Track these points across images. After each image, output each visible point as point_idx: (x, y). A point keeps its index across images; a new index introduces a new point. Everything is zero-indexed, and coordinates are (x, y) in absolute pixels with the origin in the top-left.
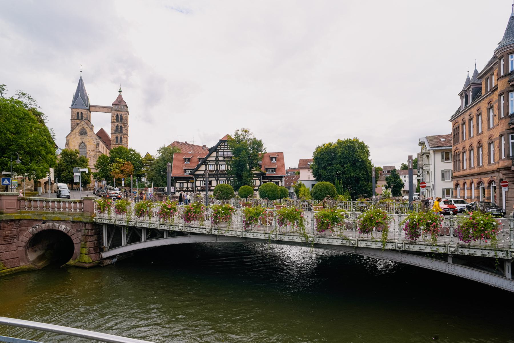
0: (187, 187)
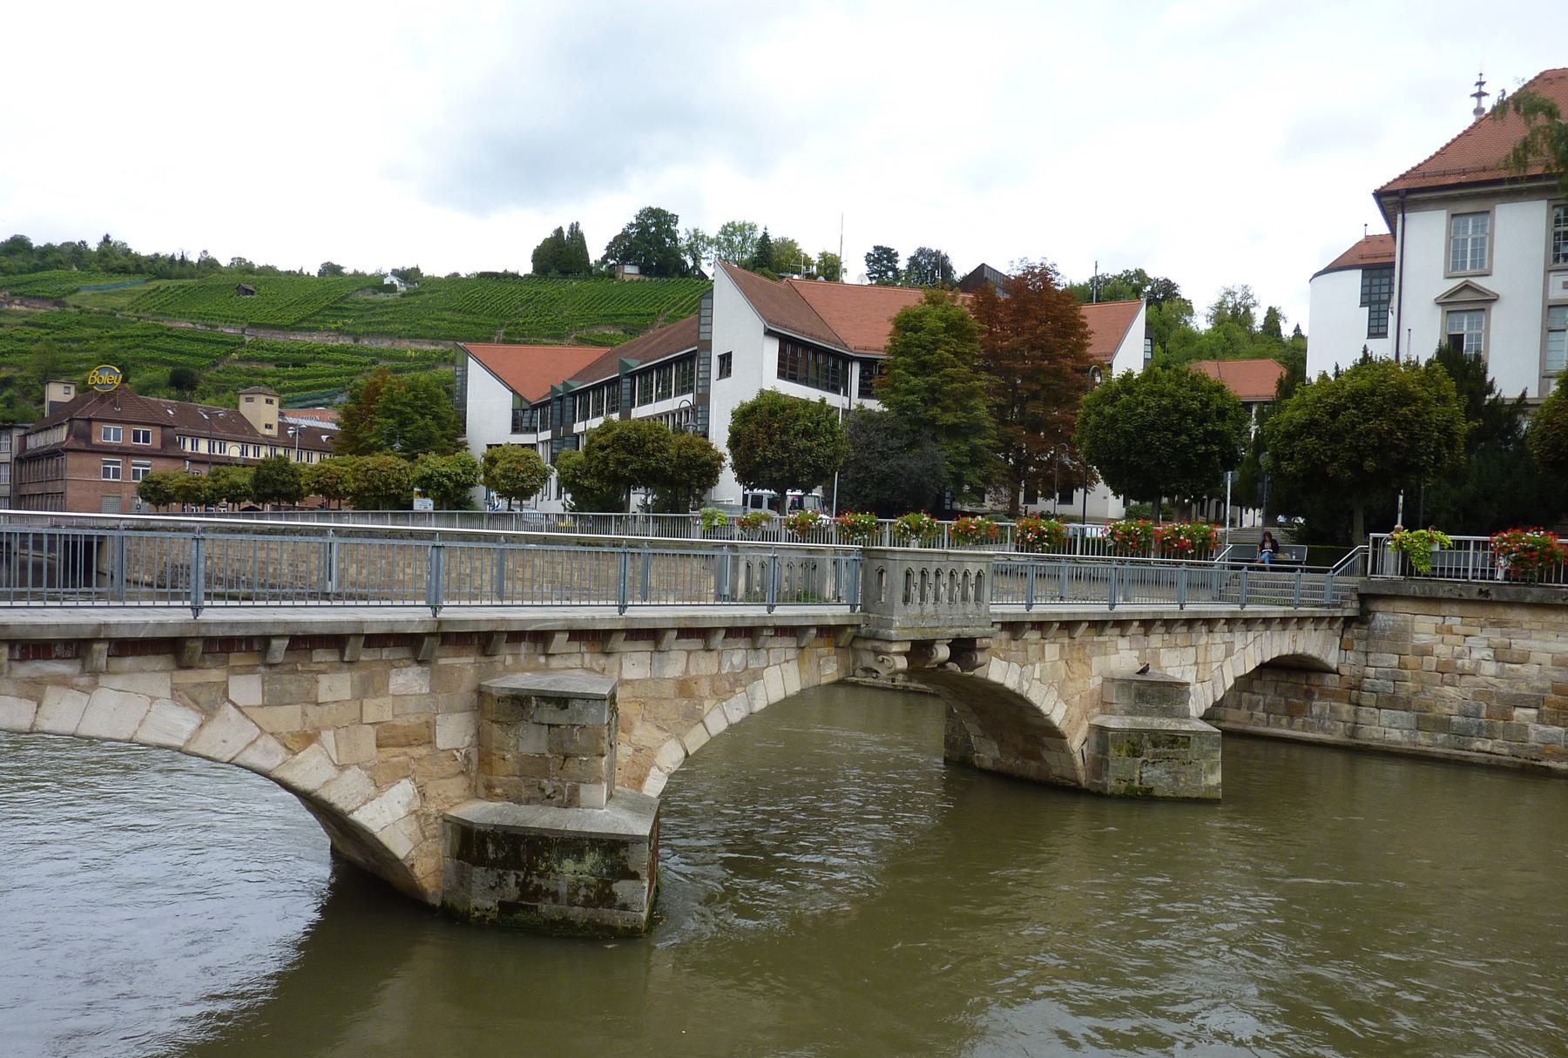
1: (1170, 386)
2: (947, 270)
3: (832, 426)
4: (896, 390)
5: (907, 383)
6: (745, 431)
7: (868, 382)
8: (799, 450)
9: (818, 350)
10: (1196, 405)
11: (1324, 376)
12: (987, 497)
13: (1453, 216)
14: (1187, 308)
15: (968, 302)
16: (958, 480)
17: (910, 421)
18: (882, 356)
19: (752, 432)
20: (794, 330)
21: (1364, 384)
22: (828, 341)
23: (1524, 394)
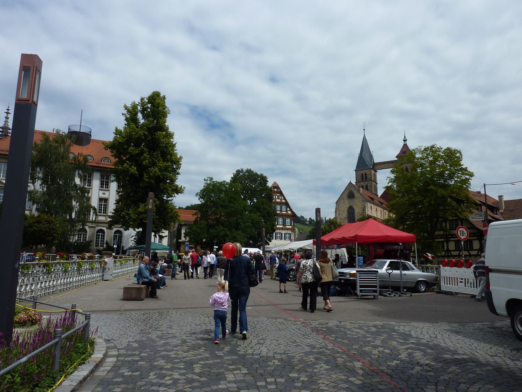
0: (448, 250)
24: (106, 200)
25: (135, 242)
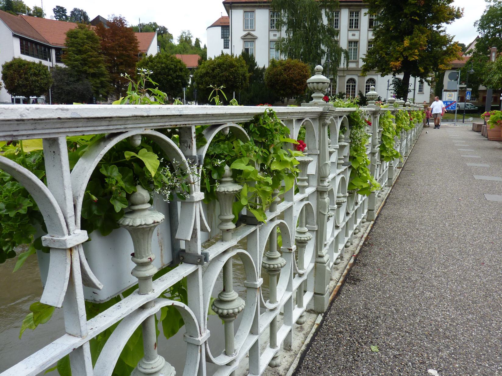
1: (164, 60)
2: (86, 18)
3: (45, 72)
4: (70, 60)
5: (74, 57)
6: (9, 73)
7: (59, 57)
8: (33, 81)
9: (37, 44)
10: (173, 67)
11: (211, 59)
12: (108, 99)
13: (245, 12)
14: (171, 37)
15: (94, 29)
16: (97, 93)
17: (77, 71)
18: (64, 47)
19: (12, 74)
20: (26, 35)
21: (221, 61)
22: (41, 40)
23: (264, 67)
24: (356, 42)
25: (395, 91)
